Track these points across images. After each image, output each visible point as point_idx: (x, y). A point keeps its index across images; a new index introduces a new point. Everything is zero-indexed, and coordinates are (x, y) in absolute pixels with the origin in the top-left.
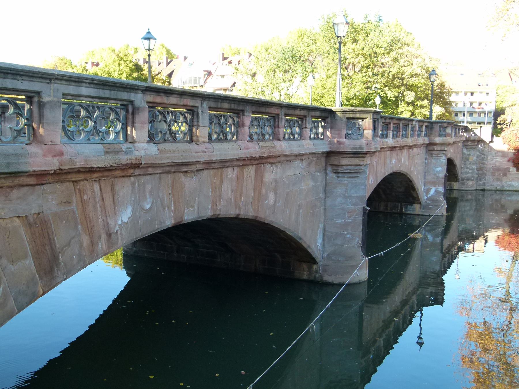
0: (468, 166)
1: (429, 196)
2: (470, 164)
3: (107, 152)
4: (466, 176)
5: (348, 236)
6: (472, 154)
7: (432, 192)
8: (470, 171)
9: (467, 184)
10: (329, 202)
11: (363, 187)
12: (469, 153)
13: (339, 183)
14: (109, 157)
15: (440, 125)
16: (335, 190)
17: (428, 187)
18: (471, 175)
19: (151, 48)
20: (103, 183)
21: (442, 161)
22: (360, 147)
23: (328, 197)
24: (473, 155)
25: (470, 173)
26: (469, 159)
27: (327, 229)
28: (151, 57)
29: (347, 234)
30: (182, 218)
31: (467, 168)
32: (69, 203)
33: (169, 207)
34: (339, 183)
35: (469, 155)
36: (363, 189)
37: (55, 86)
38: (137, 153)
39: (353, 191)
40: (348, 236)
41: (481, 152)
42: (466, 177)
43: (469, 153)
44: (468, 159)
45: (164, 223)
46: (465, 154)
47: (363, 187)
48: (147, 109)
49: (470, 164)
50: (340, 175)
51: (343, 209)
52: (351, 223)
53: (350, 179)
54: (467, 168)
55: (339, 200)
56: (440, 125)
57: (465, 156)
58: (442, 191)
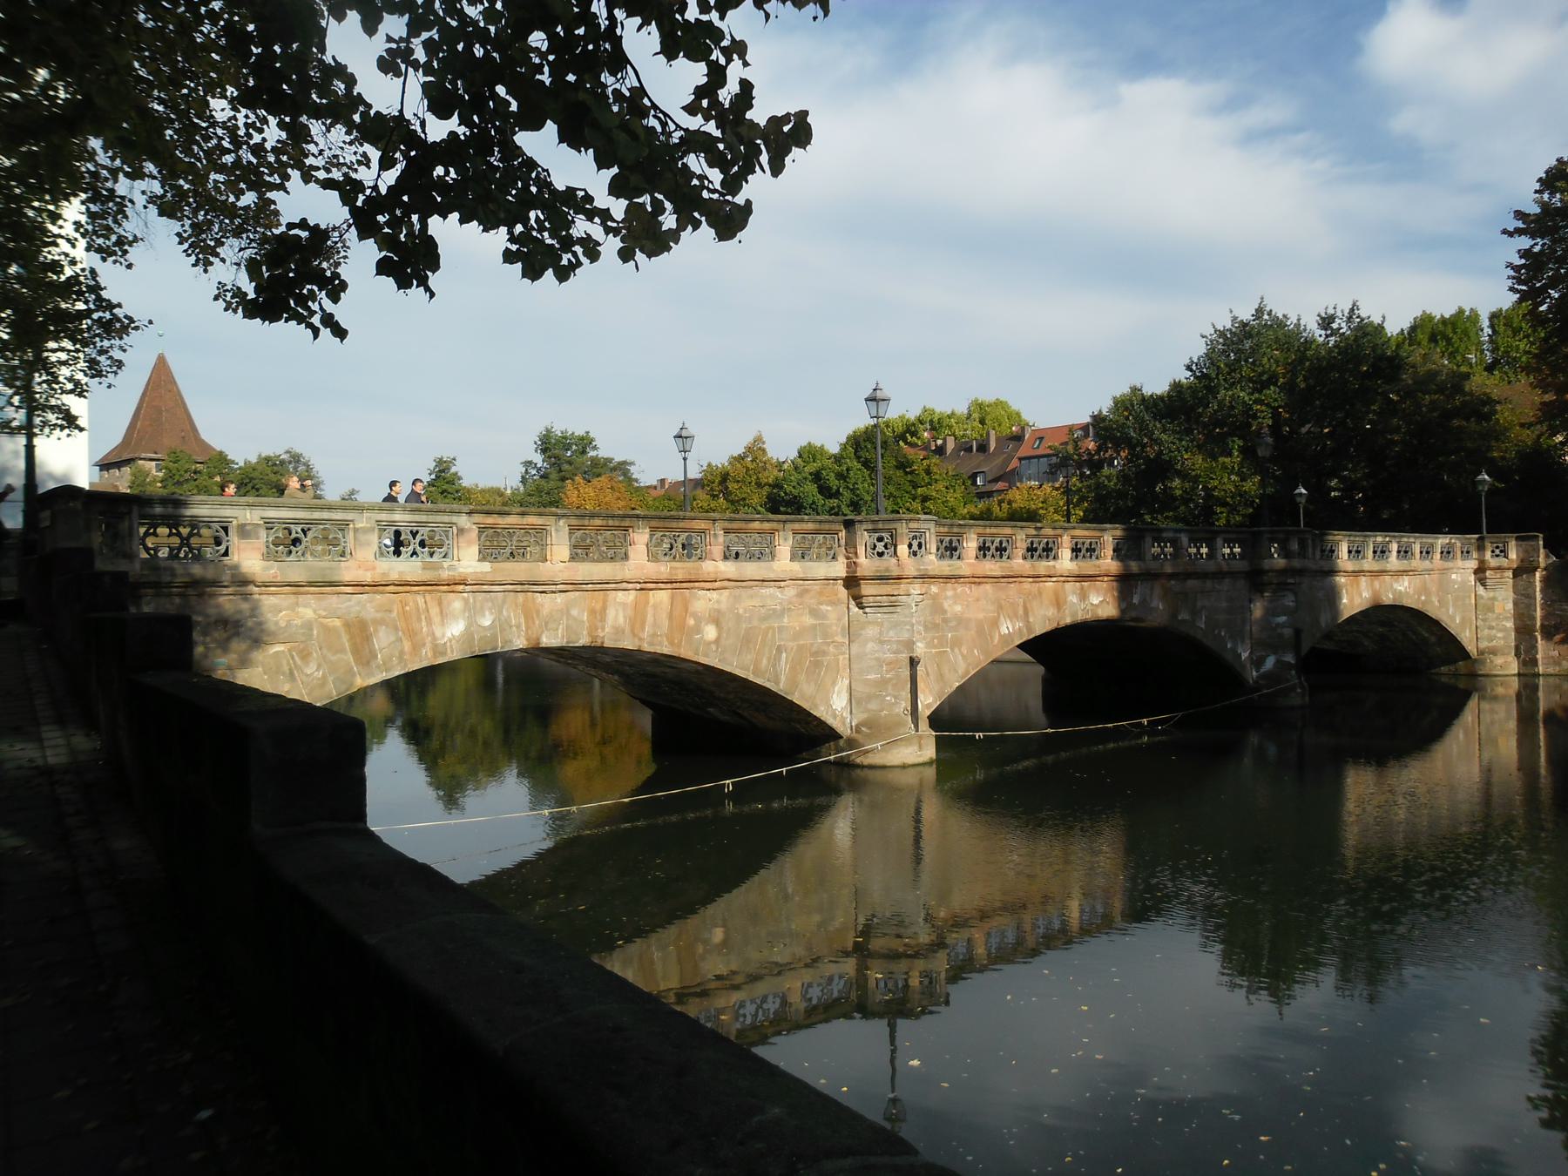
0: (1494, 624)
1: (1262, 671)
2: (1498, 618)
3: (424, 569)
4: (1490, 645)
5: (888, 698)
6: (1500, 598)
7: (1270, 662)
8: (1500, 635)
9: (1492, 662)
10: (855, 648)
11: (908, 627)
12: (1491, 594)
13: (870, 623)
14: (428, 572)
15: (1269, 536)
16: (863, 632)
17: (1258, 654)
18: (1502, 642)
19: (688, 449)
20: (428, 597)
21: (1287, 603)
22: (887, 570)
23: (853, 641)
24: (1503, 600)
25: (1499, 638)
26: (1493, 607)
27: (853, 688)
28: (688, 461)
29: (887, 696)
30: (538, 639)
31: (1491, 628)
32: (390, 611)
33: (518, 627)
34: (870, 623)
35: (1494, 599)
36: (908, 630)
37: (366, 514)
38: (461, 570)
39: (891, 633)
40: (888, 698)
41: (1523, 592)
42: (1488, 647)
43: (1491, 594)
44: (1491, 609)
45: (511, 641)
46: (1482, 597)
47: (908, 627)
48: (477, 532)
49: (1498, 618)
50: (867, 610)
51: (877, 659)
52: (890, 679)
53: (886, 616)
54: (1491, 628)
55: (870, 645)
56: (1269, 536)
57: (1482, 601)
58: (1293, 662)
